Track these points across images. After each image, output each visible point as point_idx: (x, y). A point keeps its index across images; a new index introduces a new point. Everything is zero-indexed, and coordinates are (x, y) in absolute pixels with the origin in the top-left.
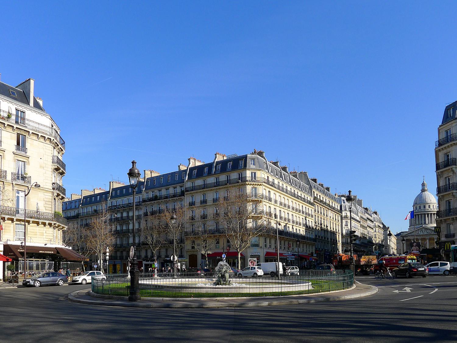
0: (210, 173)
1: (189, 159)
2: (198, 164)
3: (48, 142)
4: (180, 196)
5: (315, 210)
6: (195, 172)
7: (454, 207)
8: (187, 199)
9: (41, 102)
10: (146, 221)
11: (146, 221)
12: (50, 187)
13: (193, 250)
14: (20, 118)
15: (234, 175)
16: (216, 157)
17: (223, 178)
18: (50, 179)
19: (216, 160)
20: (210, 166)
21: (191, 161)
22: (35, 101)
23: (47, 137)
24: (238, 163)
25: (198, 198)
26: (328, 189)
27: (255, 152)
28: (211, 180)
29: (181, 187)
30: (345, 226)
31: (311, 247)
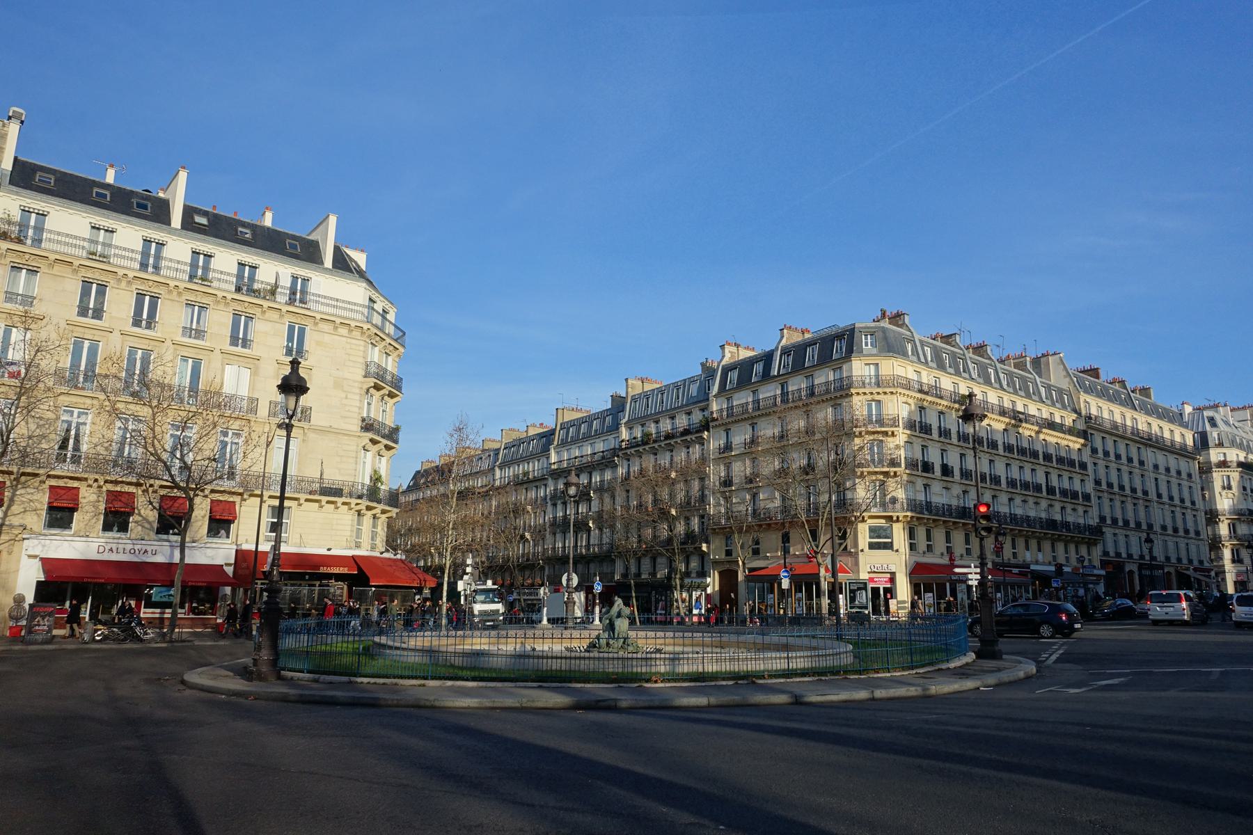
0: (766, 376)
1: (722, 347)
2: (744, 354)
3: (357, 334)
4: (697, 432)
5: (1094, 451)
6: (733, 376)
7: (364, 306)
8: (714, 441)
9: (360, 258)
10: (628, 491)
11: (628, 491)
12: (355, 426)
13: (729, 558)
14: (298, 294)
15: (824, 377)
16: (782, 337)
17: (797, 384)
18: (356, 410)
19: (784, 342)
20: (767, 358)
21: (727, 349)
22: (337, 250)
23: (353, 324)
24: (836, 346)
25: (740, 437)
26: (1145, 391)
27: (884, 315)
28: (770, 392)
29: (703, 410)
30: (1224, 488)
31: (1072, 548)
